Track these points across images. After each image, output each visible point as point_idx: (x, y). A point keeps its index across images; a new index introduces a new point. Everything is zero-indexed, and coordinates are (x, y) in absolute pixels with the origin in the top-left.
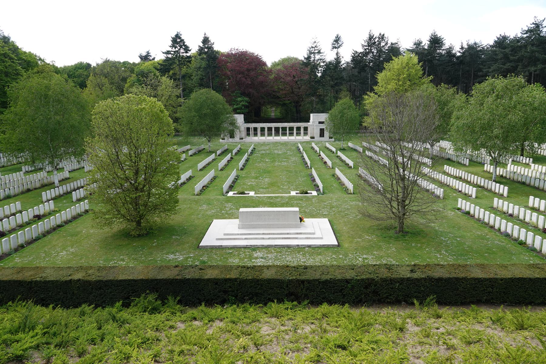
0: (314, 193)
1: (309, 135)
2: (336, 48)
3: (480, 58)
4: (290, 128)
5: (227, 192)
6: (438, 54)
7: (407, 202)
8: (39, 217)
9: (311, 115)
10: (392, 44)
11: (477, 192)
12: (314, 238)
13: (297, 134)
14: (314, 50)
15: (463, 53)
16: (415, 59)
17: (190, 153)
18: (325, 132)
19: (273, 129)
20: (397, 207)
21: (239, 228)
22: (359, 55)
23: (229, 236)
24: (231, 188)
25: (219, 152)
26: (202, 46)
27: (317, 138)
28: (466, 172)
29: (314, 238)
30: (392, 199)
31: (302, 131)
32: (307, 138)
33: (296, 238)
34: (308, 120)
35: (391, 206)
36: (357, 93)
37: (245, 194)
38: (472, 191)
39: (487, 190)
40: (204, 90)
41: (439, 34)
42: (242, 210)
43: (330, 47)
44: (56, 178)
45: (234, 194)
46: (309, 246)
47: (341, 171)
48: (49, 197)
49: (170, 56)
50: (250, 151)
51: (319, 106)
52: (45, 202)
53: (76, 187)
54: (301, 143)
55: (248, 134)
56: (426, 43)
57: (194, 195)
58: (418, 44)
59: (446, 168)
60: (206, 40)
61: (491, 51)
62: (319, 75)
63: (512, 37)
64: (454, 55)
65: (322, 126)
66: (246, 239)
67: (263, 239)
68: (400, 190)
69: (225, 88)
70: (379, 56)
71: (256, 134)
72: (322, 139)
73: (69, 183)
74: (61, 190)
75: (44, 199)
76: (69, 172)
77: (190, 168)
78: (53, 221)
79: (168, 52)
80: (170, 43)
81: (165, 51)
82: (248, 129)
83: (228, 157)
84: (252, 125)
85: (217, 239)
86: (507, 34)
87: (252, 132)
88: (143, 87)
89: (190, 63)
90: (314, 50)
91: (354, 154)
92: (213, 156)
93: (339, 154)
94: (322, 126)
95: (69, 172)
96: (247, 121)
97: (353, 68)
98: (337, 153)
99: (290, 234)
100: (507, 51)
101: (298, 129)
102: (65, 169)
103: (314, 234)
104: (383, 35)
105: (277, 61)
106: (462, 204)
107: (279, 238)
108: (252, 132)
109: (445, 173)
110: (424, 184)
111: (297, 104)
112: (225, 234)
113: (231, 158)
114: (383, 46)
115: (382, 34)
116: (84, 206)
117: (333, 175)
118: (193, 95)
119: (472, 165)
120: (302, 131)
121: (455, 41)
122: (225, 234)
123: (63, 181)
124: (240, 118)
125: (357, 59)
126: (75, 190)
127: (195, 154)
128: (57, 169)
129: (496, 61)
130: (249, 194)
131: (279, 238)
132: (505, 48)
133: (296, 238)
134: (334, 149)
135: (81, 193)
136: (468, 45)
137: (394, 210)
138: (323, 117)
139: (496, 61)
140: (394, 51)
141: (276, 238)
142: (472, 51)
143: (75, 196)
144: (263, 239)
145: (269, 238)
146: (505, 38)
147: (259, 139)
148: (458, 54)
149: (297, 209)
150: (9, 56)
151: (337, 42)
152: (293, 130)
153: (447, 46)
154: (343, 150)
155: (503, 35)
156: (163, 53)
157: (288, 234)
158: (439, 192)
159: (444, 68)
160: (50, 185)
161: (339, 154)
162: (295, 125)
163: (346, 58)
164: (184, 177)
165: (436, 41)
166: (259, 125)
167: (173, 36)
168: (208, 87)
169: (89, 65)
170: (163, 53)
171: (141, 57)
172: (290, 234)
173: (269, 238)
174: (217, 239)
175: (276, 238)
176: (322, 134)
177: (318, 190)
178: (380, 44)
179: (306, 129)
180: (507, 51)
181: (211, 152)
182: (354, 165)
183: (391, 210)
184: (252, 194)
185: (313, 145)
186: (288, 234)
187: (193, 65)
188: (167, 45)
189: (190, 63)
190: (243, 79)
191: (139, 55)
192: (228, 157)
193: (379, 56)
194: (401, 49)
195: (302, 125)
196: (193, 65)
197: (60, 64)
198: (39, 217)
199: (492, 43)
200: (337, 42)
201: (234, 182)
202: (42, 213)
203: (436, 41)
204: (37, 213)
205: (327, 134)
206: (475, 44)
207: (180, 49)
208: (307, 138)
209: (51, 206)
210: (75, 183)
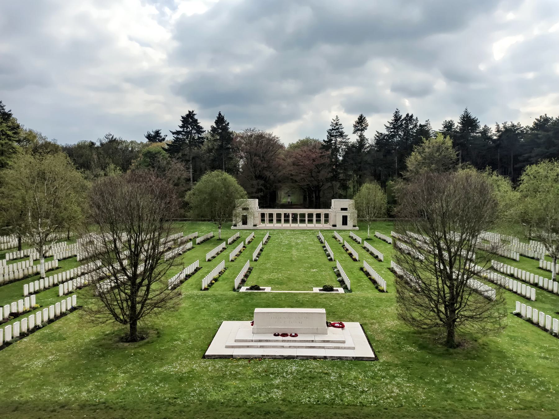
0: (341, 290)
1: (331, 222)
2: (359, 130)
3: (519, 141)
4: (300, 214)
5: (239, 288)
6: (473, 137)
7: (457, 306)
8: (15, 316)
9: (333, 201)
10: (421, 126)
11: (537, 294)
12: (345, 348)
13: (317, 221)
14: (336, 131)
15: (500, 136)
16: (449, 142)
17: (198, 240)
18: (348, 219)
19: (307, 216)
20: (444, 312)
21: (253, 333)
22: (384, 138)
23: (241, 343)
24: (243, 282)
25: (230, 241)
26: (215, 126)
27: (340, 226)
28: (519, 268)
29: (345, 348)
30: (438, 302)
31: (323, 218)
32: (328, 226)
33: (323, 348)
34: (328, 206)
35: (438, 310)
36: (383, 178)
37: (260, 289)
38: (531, 293)
39: (547, 290)
40: (215, 173)
41: (473, 116)
42: (257, 310)
43: (353, 129)
44: (43, 267)
45: (247, 289)
46: (340, 358)
47: (371, 264)
48: (32, 290)
49: (180, 136)
50: (265, 239)
51: (341, 192)
52: (27, 296)
53: (68, 277)
54: (322, 231)
55: (263, 221)
56: (457, 124)
57: (201, 290)
58: (449, 126)
59: (493, 263)
60: (220, 114)
61: (531, 134)
62: (341, 158)
63: (554, 119)
64: (490, 138)
65: (344, 213)
66: (262, 347)
67: (283, 347)
68: (447, 290)
69: (239, 171)
70: (407, 139)
71: (271, 221)
72: (345, 227)
73: (62, 272)
74: (47, 282)
75: (26, 293)
76: (59, 260)
77: (197, 257)
78: (31, 321)
79: (178, 133)
80: (181, 124)
81: (174, 131)
82: (263, 215)
83: (240, 247)
84: (267, 211)
85: (227, 347)
86: (549, 116)
87: (267, 218)
88: (149, 169)
89: (203, 145)
90: (336, 131)
91: (382, 244)
92: (223, 245)
93: (366, 244)
94: (344, 213)
95: (59, 260)
96: (261, 206)
97: (377, 151)
98: (363, 243)
99: (316, 342)
100: (550, 133)
101: (318, 215)
102: (55, 258)
103: (344, 342)
104: (412, 116)
105: (295, 142)
106: (520, 307)
107: (302, 347)
108: (267, 218)
109: (492, 268)
110: (474, 283)
111: (318, 188)
112: (236, 341)
113: (244, 247)
114: (411, 129)
115: (410, 115)
116: (73, 301)
117: (362, 269)
118: (204, 177)
119: (524, 261)
120: (323, 218)
121: (491, 122)
122: (236, 341)
123: (50, 271)
124: (254, 203)
125: (381, 140)
126: (63, 282)
127: (202, 242)
128: (45, 257)
129: (539, 145)
130: (264, 289)
131: (302, 347)
132: (547, 130)
133: (323, 348)
134: (359, 239)
135: (70, 286)
136: (504, 127)
137: (442, 316)
138: (347, 203)
139: (539, 145)
140: (424, 132)
141: (299, 347)
142: (510, 133)
143: (62, 289)
144: (283, 347)
145: (290, 347)
146: (546, 120)
147: (275, 225)
148: (495, 138)
149: (323, 311)
150: (6, 133)
151: (361, 124)
152: (305, 217)
153: (482, 127)
154: (368, 240)
155: (543, 115)
156: (173, 133)
157: (313, 341)
158: (492, 293)
159: (479, 152)
160: (37, 276)
161: (366, 244)
162: (314, 211)
163: (370, 136)
164: (189, 270)
165: (468, 122)
166: (275, 211)
167: (184, 115)
168: (222, 169)
169: (93, 144)
170: (173, 133)
171: (149, 137)
172: (316, 342)
173: (290, 347)
174: (227, 347)
175: (299, 347)
176: (345, 221)
177: (346, 288)
178: (407, 127)
179: (327, 216)
180: (550, 133)
181: (220, 240)
182: (384, 257)
183: (439, 316)
184: (268, 289)
185: (336, 234)
186: (313, 341)
187: (204, 148)
188: (177, 124)
189: (203, 145)
190: (259, 162)
191: (146, 134)
192: (240, 247)
193: (407, 139)
194: (431, 132)
195: (322, 211)
196: (204, 148)
197: (62, 142)
198: (15, 316)
199: (531, 125)
200: (361, 124)
201: (246, 276)
202: (21, 310)
203: (468, 122)
204: (14, 310)
205: (350, 222)
206: (513, 126)
207: (191, 130)
208: (328, 226)
209: (33, 301)
210: (64, 273)
